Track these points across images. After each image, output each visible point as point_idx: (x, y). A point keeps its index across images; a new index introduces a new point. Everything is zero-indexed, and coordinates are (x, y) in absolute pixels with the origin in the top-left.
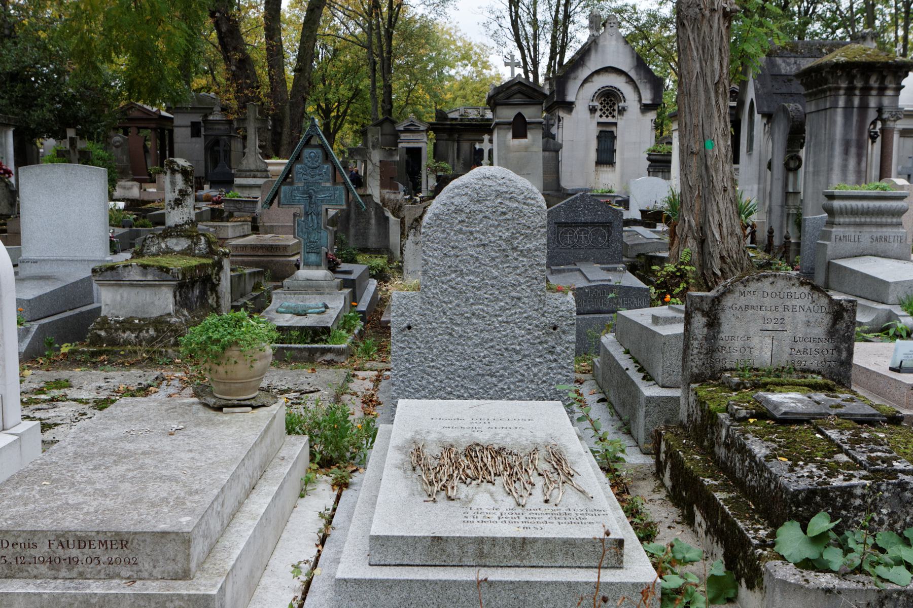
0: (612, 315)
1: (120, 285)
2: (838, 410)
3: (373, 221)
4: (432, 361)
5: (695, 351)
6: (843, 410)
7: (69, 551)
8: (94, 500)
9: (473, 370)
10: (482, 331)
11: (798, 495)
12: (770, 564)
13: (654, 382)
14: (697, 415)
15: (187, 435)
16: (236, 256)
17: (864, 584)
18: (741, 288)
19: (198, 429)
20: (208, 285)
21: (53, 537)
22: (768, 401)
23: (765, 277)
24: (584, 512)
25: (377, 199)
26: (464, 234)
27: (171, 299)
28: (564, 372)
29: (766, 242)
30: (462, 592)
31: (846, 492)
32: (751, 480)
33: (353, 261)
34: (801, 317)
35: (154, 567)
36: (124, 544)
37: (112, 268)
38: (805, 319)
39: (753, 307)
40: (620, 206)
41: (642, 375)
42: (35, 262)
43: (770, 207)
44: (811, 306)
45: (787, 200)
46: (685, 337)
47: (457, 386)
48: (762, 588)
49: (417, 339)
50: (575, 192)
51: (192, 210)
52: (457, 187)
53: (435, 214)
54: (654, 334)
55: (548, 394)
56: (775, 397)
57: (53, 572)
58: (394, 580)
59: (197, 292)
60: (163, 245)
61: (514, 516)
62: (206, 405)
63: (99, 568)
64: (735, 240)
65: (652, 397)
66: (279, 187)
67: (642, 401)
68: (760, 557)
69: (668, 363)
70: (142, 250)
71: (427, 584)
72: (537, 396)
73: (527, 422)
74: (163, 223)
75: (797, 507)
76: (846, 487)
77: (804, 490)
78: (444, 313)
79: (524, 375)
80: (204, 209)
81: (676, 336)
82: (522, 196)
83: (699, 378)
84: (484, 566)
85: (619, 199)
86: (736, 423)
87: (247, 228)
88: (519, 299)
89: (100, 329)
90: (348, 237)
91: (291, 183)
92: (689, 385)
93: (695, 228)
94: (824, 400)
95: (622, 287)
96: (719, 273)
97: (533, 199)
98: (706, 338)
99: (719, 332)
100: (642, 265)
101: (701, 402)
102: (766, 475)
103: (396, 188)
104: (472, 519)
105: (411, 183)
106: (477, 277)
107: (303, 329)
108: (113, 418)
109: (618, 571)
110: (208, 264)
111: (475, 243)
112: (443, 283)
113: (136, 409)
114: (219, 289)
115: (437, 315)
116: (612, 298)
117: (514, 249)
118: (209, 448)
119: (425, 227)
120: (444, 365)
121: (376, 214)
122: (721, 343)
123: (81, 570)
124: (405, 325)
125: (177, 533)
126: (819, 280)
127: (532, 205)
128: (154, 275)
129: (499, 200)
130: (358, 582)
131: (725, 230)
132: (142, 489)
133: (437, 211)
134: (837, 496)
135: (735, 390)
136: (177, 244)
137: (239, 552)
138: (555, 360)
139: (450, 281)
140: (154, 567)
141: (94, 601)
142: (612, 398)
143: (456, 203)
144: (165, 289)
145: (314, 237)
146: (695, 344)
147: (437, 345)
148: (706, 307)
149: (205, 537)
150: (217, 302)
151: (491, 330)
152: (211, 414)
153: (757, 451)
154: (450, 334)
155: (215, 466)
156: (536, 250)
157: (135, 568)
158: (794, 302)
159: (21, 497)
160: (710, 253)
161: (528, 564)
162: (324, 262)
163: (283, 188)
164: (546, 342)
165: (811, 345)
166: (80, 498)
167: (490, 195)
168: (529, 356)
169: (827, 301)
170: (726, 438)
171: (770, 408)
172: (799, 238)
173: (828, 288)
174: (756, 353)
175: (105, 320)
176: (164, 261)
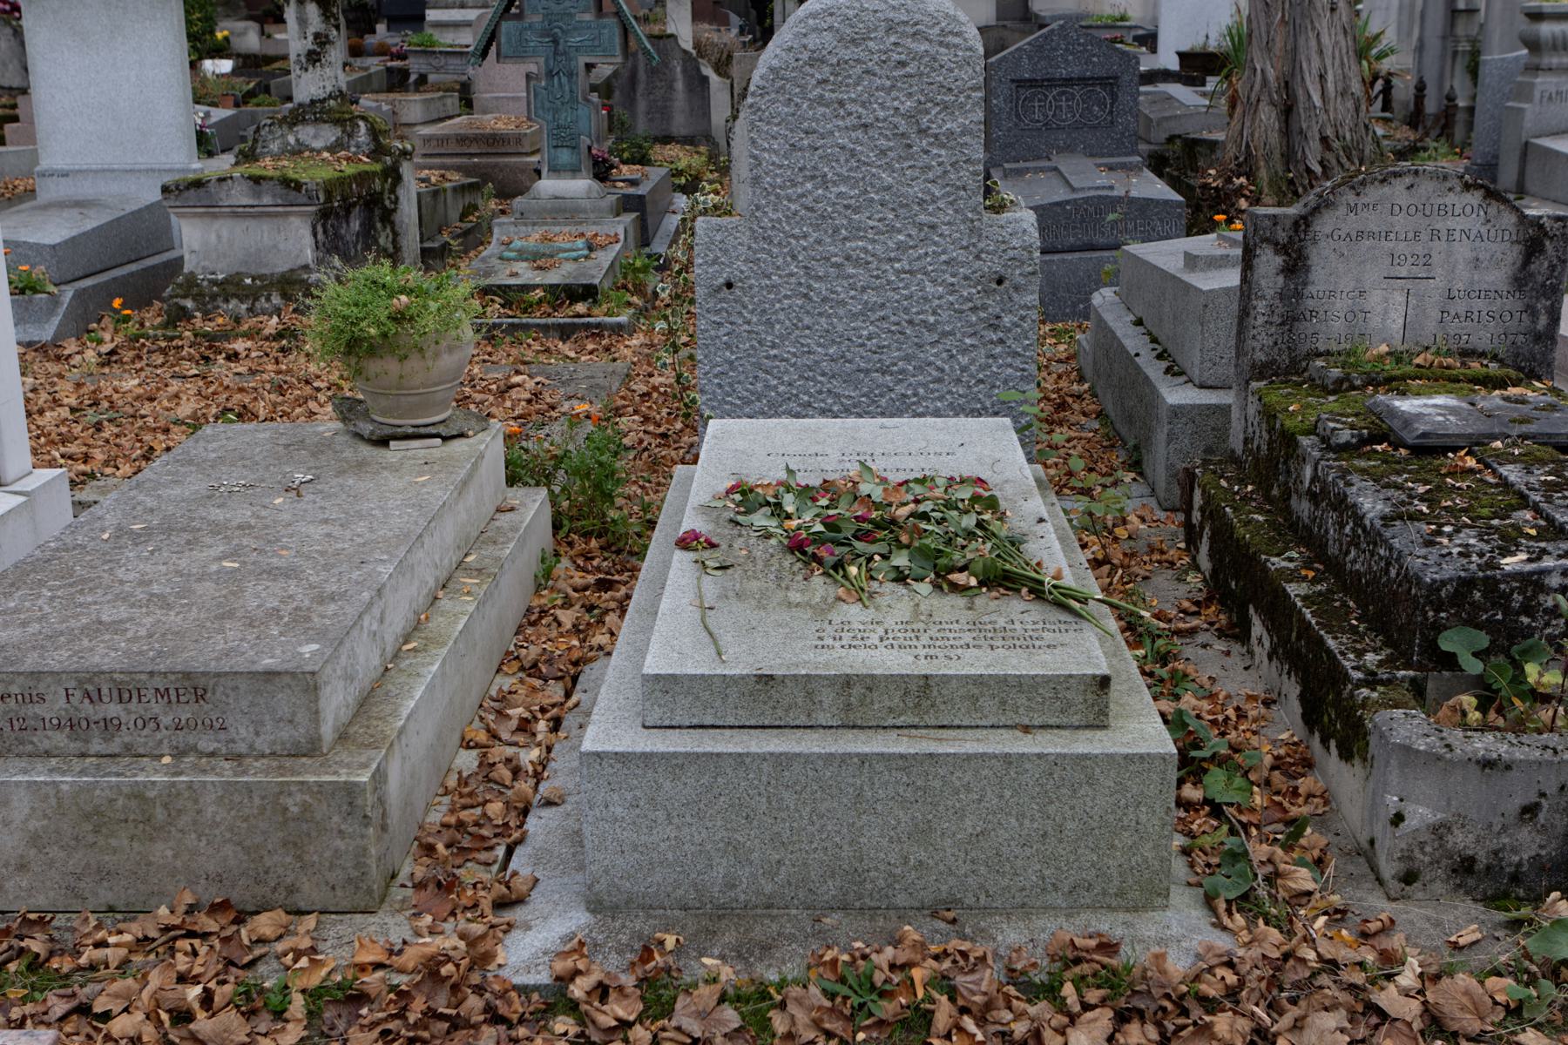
0: (1115, 253)
1: (214, 216)
2: (1525, 428)
3: (680, 85)
4: (774, 346)
5: (1261, 320)
6: (1532, 428)
7: (104, 707)
8: (148, 614)
9: (850, 362)
10: (864, 289)
11: (1439, 590)
12: (1382, 716)
13: (1183, 379)
14: (1261, 440)
15: (321, 492)
16: (457, 155)
17: (1555, 752)
18: (1350, 197)
19: (340, 480)
20: (377, 212)
21: (73, 684)
22: (1393, 413)
23: (1396, 175)
24: (1040, 626)
25: (687, 43)
26: (827, 106)
27: (308, 240)
28: (1017, 362)
29: (1412, 106)
30: (810, 773)
31: (1532, 582)
32: (1354, 561)
33: (644, 160)
34: (1463, 251)
35: (257, 734)
36: (200, 695)
37: (198, 184)
38: (1469, 255)
39: (1372, 235)
40: (1141, 45)
41: (1164, 364)
42: (65, 174)
43: (1421, 40)
44: (1484, 230)
45: (1453, 25)
46: (1242, 294)
47: (820, 392)
48: (1365, 760)
49: (745, 307)
50: (1055, 18)
51: (340, 72)
52: (814, 15)
53: (771, 69)
54: (1188, 287)
55: (988, 404)
56: (1406, 405)
57: (78, 744)
58: (687, 755)
59: (356, 225)
60: (291, 139)
61: (909, 634)
62: (358, 436)
63: (159, 736)
64: (1350, 104)
65: (1180, 407)
66: (497, 25)
67: (1164, 414)
68: (1365, 703)
69: (1208, 346)
70: (253, 149)
71: (748, 761)
72: (968, 407)
73: (944, 458)
74: (290, 99)
75: (1437, 611)
76: (1531, 573)
77: (1451, 579)
78: (794, 257)
79: (943, 370)
80: (373, 70)
81: (1227, 291)
82: (937, 30)
83: (1262, 371)
84: (854, 727)
85: (1140, 32)
86: (1332, 455)
87: (453, 102)
88: (933, 227)
89: (185, 297)
90: (633, 115)
91: (519, 17)
92: (1247, 383)
93: (1273, 84)
94: (1499, 408)
95: (1133, 201)
96: (1318, 169)
97: (957, 34)
98: (1281, 296)
99: (1305, 284)
100: (1177, 158)
101: (1268, 414)
102: (1382, 552)
103: (725, 22)
104: (831, 642)
105: (753, 13)
106: (852, 188)
107: (552, 289)
108: (190, 462)
109: (1099, 734)
110: (374, 173)
111: (849, 122)
112: (790, 200)
113: (232, 444)
114: (397, 217)
115: (780, 261)
116: (1115, 222)
117: (922, 132)
118: (360, 516)
119: (753, 94)
120: (794, 355)
121: (684, 71)
122: (1310, 303)
123: (127, 739)
124: (721, 280)
125: (293, 674)
126: (1507, 177)
127: (956, 46)
128: (274, 196)
129: (893, 39)
130: (622, 758)
131: (1330, 86)
132: (233, 593)
133: (775, 63)
134: (1512, 590)
135: (1334, 392)
136: (315, 137)
137: (412, 704)
138: (1001, 341)
139: (803, 195)
140: (257, 734)
141: (151, 794)
142: (1110, 409)
143: (811, 46)
144: (295, 222)
145: (565, 117)
146: (1261, 306)
147: (782, 316)
148: (1282, 236)
149: (349, 678)
150: (394, 242)
151: (882, 286)
152: (366, 450)
153: (1367, 506)
154: (806, 296)
155: (367, 549)
156: (963, 134)
157: (222, 735)
158: (1451, 223)
159: (16, 611)
160: (1301, 132)
161: (933, 722)
162: (586, 164)
163: (506, 26)
164: (984, 308)
165: (1479, 304)
166: (123, 612)
167: (875, 30)
168: (952, 333)
169: (1513, 219)
170: (1312, 481)
171: (1396, 424)
172: (1474, 98)
173: (1521, 191)
174: (1375, 321)
175: (191, 280)
176: (290, 167)
